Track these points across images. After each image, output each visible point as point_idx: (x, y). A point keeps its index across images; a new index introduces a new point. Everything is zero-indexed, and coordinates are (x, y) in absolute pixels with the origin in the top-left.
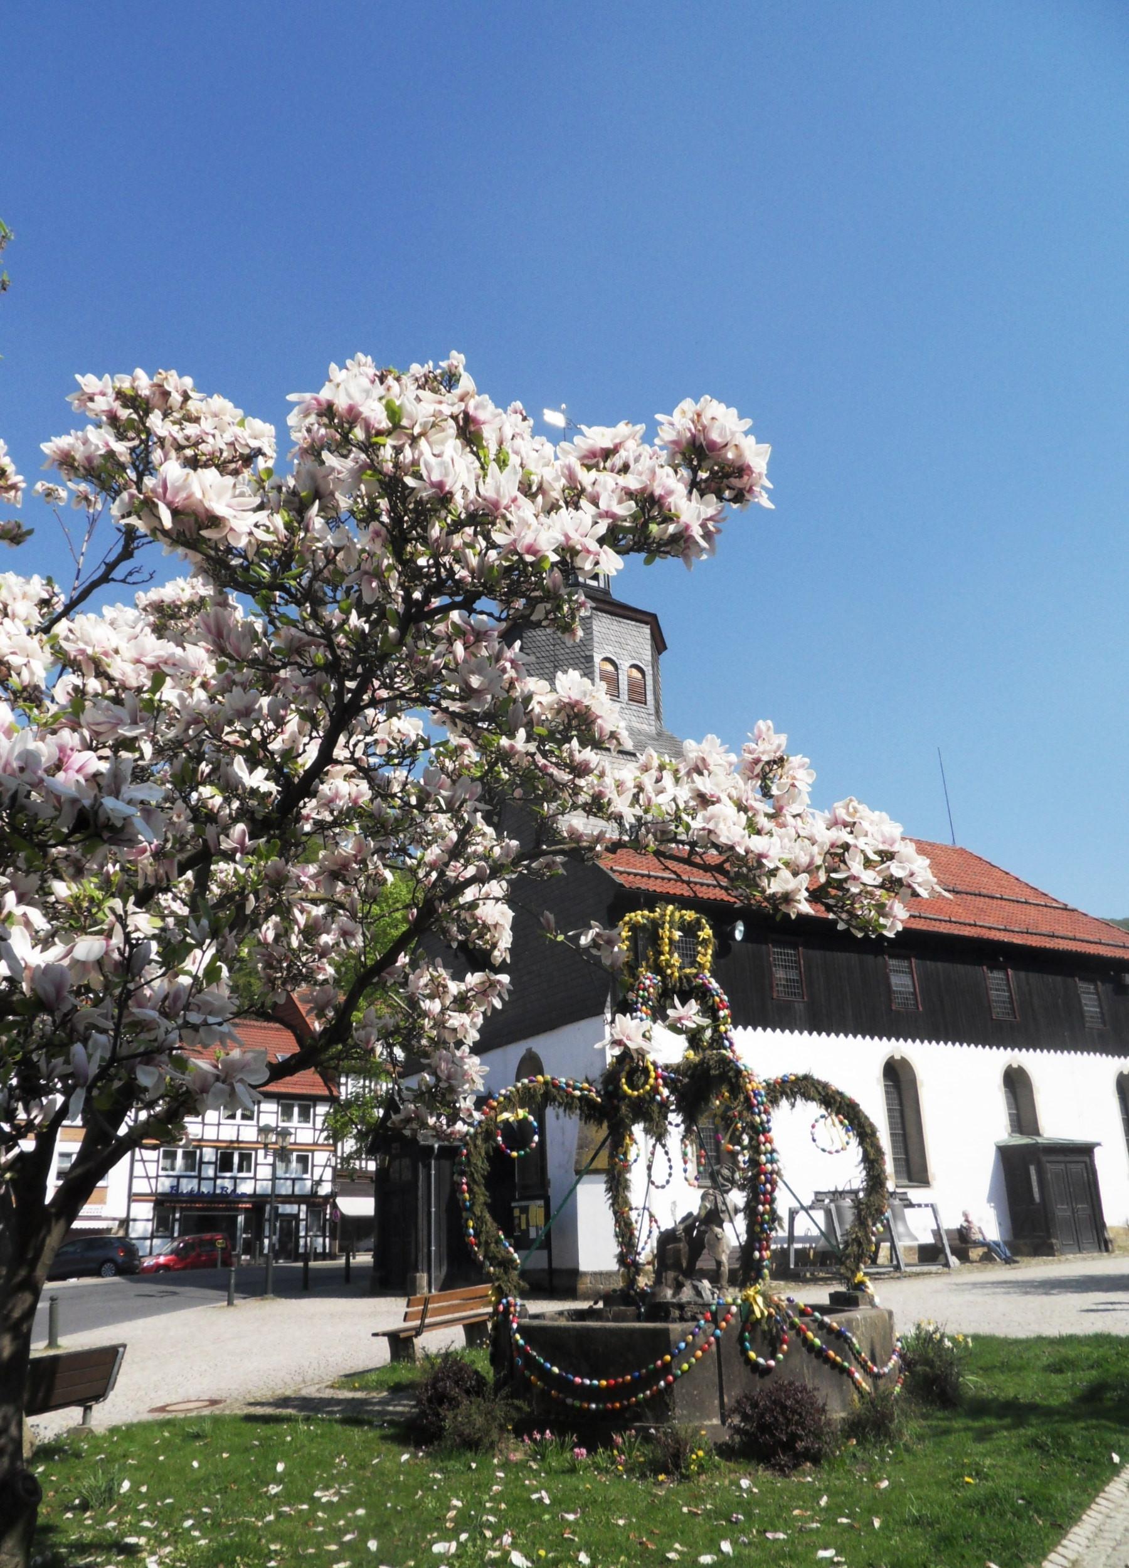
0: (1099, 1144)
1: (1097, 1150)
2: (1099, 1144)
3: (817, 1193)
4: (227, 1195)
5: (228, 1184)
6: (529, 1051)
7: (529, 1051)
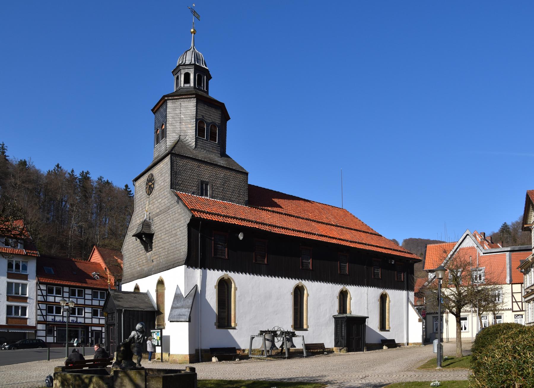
0: (368, 317)
1: (367, 319)
2: (368, 317)
3: (261, 331)
4: (74, 323)
5: (75, 319)
6: (161, 277)
7: (161, 277)
